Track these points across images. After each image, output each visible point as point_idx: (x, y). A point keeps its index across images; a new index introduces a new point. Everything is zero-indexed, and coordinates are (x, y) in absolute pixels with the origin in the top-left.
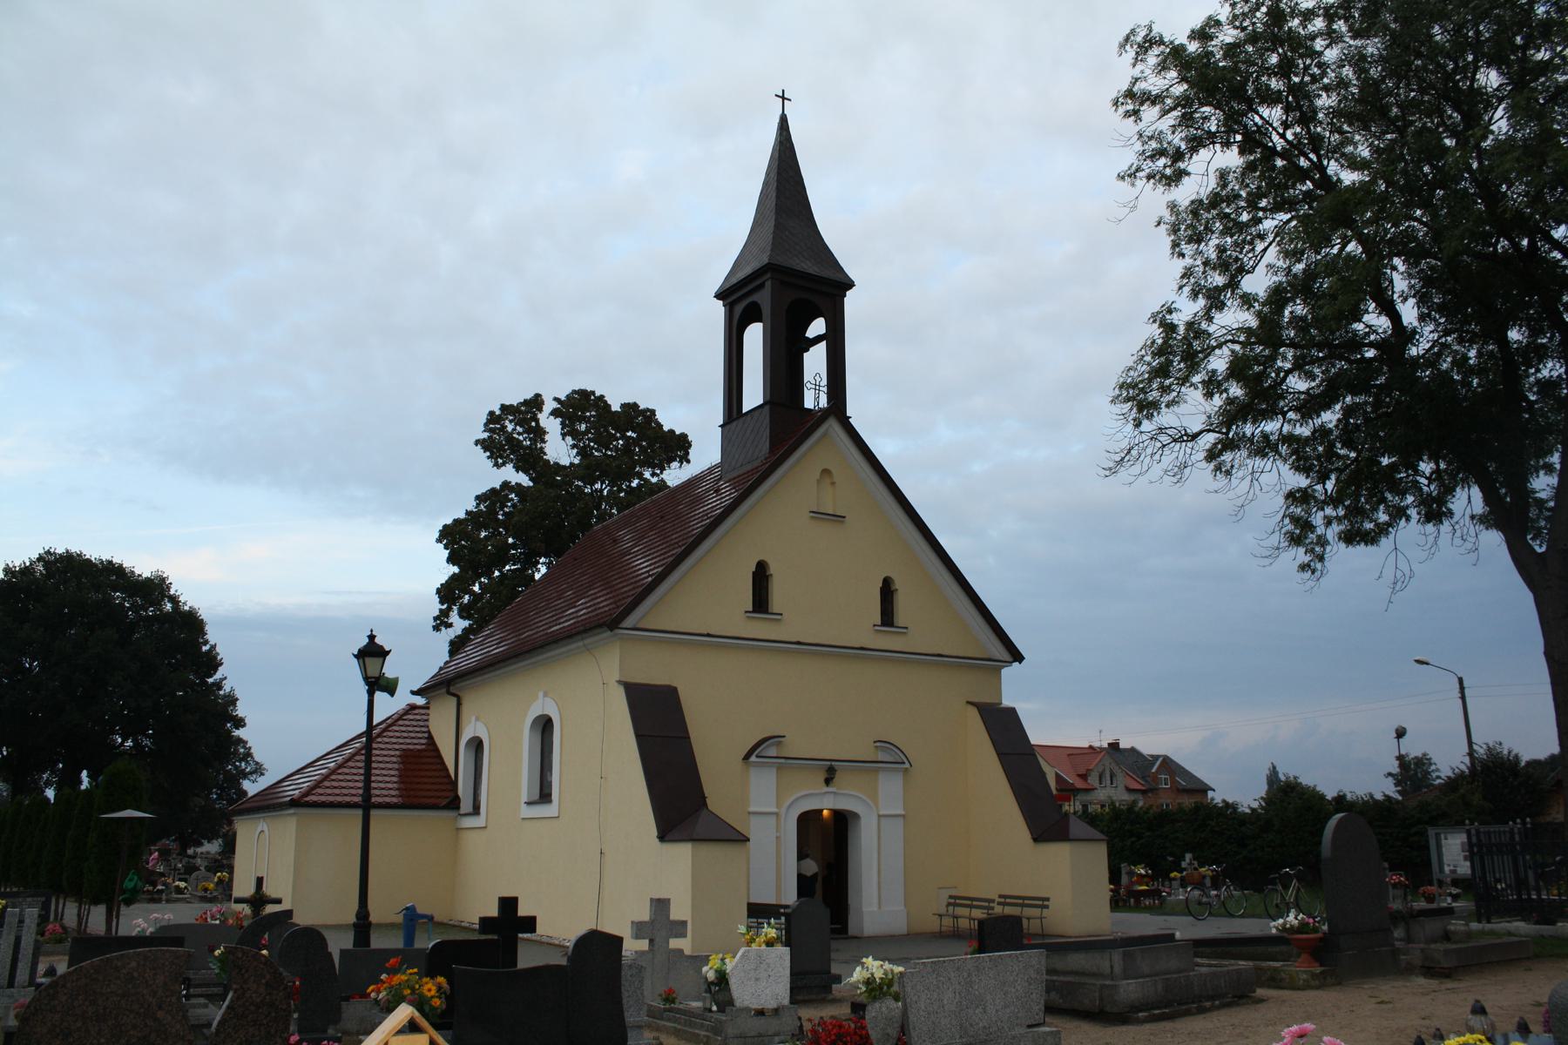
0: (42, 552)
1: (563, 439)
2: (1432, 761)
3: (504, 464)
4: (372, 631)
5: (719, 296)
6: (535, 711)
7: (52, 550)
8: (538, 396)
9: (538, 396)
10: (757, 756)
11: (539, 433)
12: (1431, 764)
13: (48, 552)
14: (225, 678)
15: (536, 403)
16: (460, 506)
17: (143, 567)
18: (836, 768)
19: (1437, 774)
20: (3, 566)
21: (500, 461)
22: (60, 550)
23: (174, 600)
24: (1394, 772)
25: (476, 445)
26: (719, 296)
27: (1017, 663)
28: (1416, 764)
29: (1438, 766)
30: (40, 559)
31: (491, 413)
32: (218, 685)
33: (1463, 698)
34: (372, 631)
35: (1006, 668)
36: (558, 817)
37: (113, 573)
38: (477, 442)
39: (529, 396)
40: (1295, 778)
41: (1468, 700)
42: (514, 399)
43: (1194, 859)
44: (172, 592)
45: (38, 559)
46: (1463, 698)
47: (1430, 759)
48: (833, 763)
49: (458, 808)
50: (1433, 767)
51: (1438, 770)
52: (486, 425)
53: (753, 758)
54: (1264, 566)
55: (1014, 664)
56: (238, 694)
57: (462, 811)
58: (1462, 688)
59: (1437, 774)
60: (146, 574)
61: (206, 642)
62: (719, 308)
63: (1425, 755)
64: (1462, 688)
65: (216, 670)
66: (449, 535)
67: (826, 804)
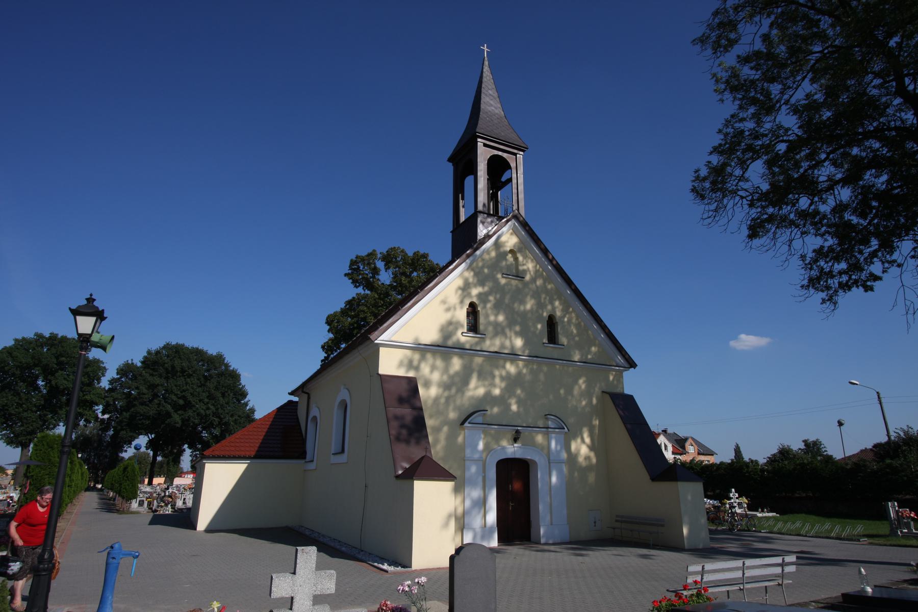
0: (165, 343)
1: (386, 271)
2: (822, 443)
3: (359, 286)
4: (91, 295)
5: (450, 160)
6: (339, 400)
7: (170, 343)
8: (374, 251)
9: (374, 251)
10: (469, 423)
11: (375, 271)
12: (821, 445)
13: (168, 344)
14: (249, 401)
15: (372, 255)
16: (338, 305)
17: (212, 351)
18: (521, 431)
19: (825, 449)
20: (147, 350)
21: (358, 284)
22: (174, 343)
23: (227, 366)
24: (802, 448)
25: (345, 276)
26: (450, 160)
27: (633, 369)
28: (813, 444)
29: (825, 445)
30: (165, 347)
31: (352, 260)
32: (246, 404)
33: (881, 403)
34: (91, 295)
35: (626, 372)
36: (347, 463)
37: (199, 353)
38: (346, 275)
39: (370, 251)
40: (788, 446)
41: (884, 405)
42: (363, 253)
43: (736, 493)
44: (226, 362)
45: (163, 347)
46: (881, 403)
47: (821, 442)
48: (519, 428)
49: (305, 458)
50: (822, 446)
51: (825, 447)
52: (350, 267)
53: (466, 424)
54: (795, 297)
55: (630, 369)
56: (256, 408)
57: (307, 460)
58: (879, 398)
59: (825, 449)
60: (215, 354)
61: (240, 384)
62: (450, 167)
63: (817, 440)
64: (879, 398)
65: (246, 397)
66: (329, 321)
67: (512, 450)
